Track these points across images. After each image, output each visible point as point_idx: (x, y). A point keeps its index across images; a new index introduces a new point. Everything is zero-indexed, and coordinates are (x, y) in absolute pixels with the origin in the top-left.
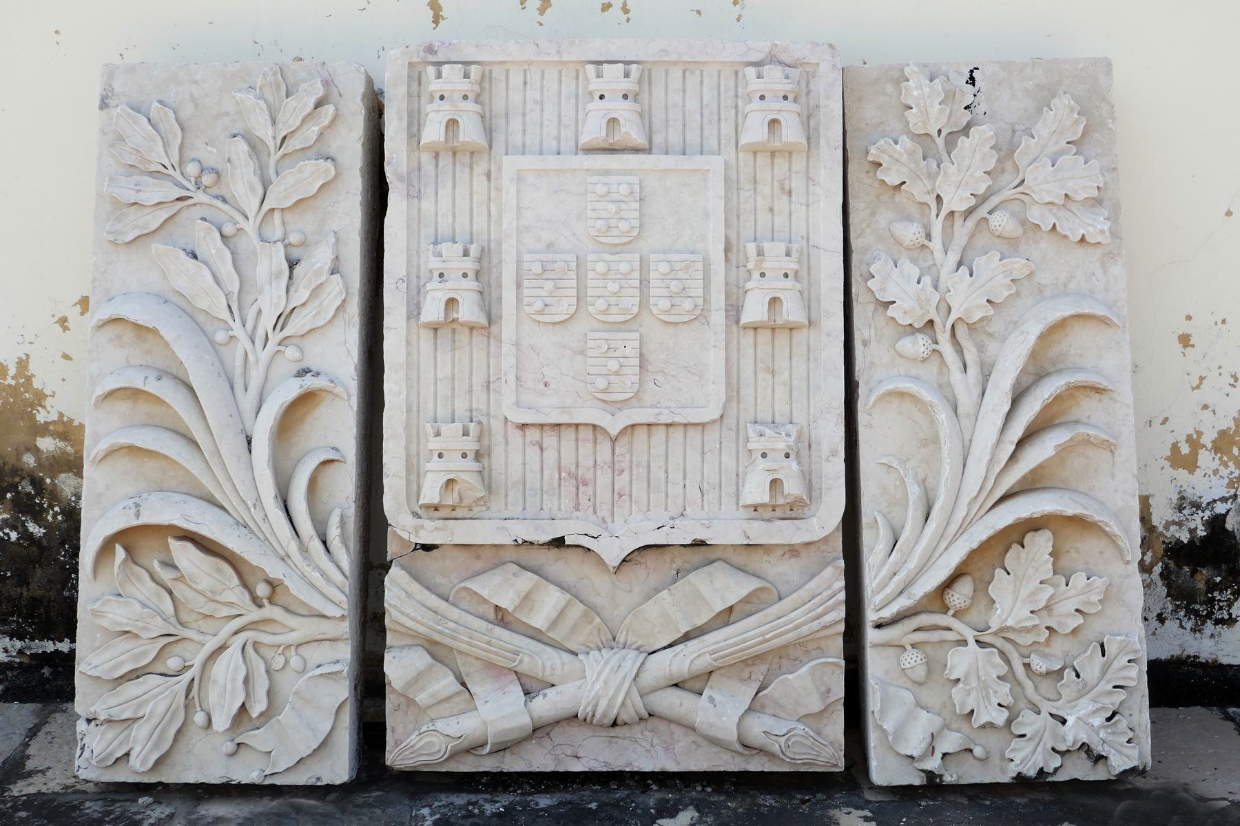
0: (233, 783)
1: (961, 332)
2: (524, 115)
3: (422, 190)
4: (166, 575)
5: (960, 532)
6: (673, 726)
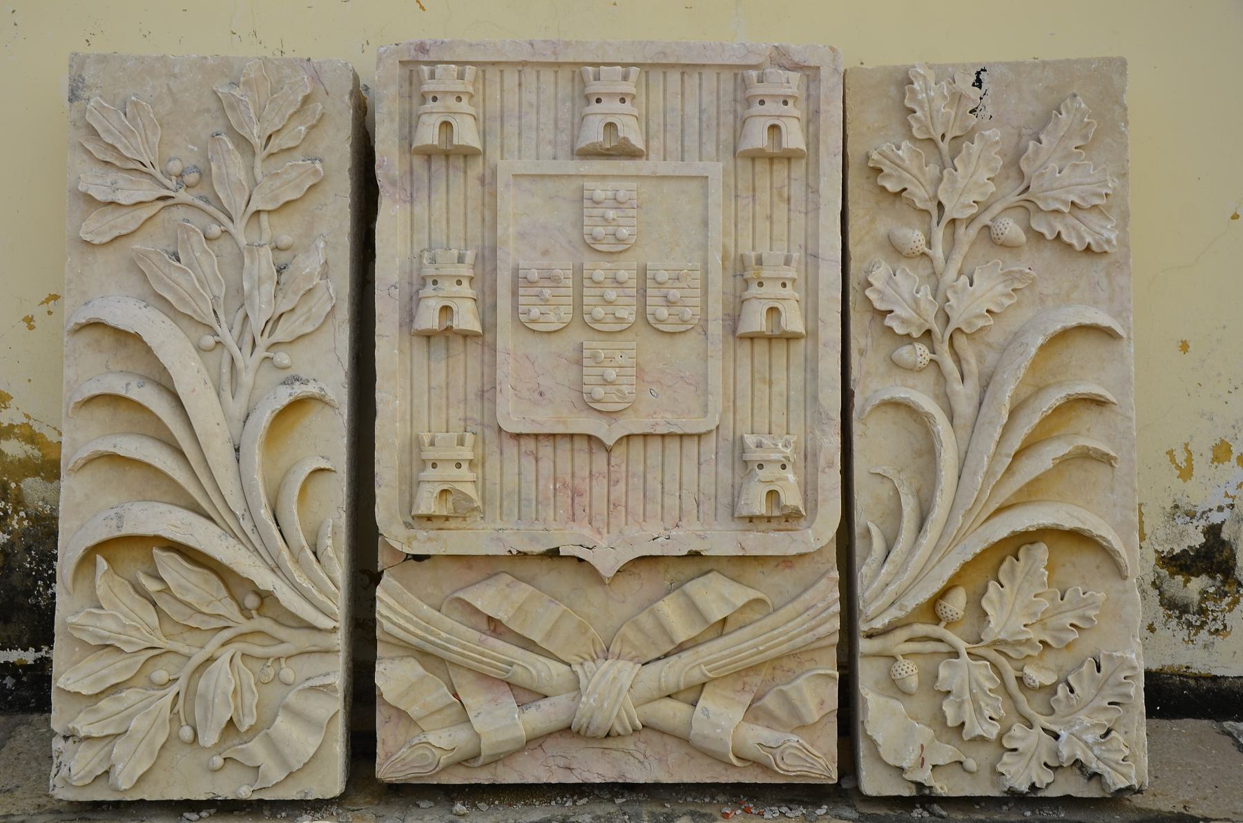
0: (219, 799)
1: (961, 341)
2: (520, 118)
3: (415, 195)
4: (152, 586)
5: (954, 544)
6: (665, 737)
